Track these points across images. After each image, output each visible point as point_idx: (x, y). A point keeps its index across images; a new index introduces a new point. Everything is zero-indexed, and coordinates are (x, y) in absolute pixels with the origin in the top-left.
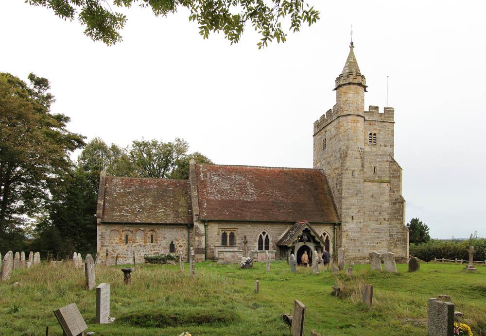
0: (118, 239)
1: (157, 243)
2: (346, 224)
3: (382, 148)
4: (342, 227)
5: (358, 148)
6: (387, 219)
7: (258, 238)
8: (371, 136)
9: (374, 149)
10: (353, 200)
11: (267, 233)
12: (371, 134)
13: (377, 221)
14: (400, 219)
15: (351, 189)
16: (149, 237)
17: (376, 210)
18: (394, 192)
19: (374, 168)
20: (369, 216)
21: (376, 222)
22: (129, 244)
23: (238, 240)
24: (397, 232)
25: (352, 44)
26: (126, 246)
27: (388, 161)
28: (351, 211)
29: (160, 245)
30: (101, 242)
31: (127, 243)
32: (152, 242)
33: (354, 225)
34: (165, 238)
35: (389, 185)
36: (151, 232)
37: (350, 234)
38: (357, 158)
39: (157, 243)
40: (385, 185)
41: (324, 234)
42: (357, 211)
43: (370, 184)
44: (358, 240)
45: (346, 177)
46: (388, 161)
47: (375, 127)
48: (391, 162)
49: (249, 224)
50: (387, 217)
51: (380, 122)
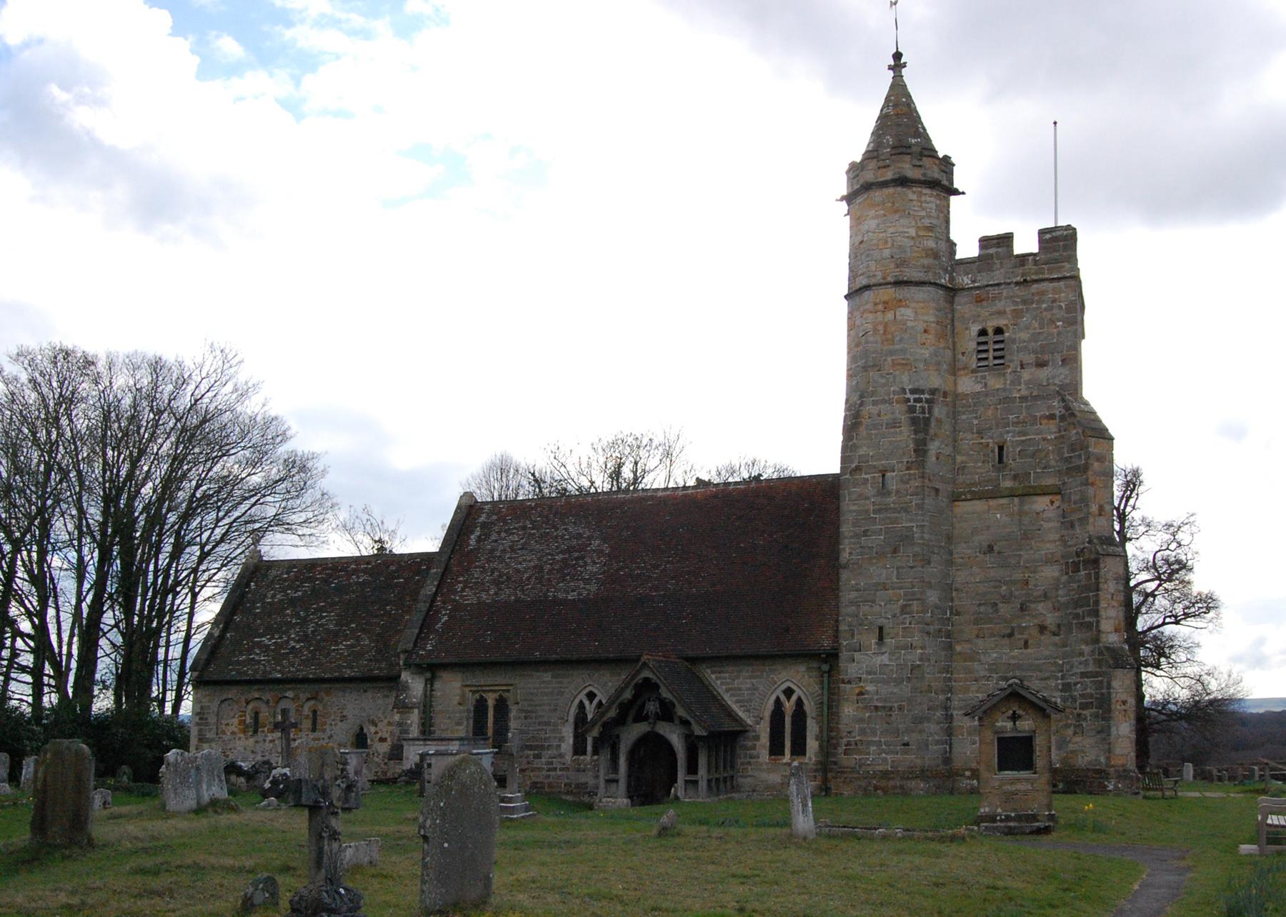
0: (236, 721)
1: (324, 731)
2: (856, 655)
3: (1026, 375)
4: (842, 665)
5: (904, 391)
6: (1053, 628)
7: (573, 710)
8: (983, 339)
9: (995, 383)
10: (881, 572)
11: (798, 692)
12: (983, 333)
13: (1010, 635)
14: (1089, 626)
15: (874, 533)
16: (307, 717)
17: (1006, 599)
18: (1072, 526)
19: (1001, 448)
20: (976, 622)
21: (1006, 641)
22: (260, 736)
23: (516, 718)
24: (1083, 675)
25: (897, 56)
26: (252, 740)
27: (1052, 417)
28: (876, 608)
29: (331, 737)
30: (200, 731)
31: (256, 732)
32: (314, 730)
33: (885, 659)
34: (343, 718)
35: (1057, 504)
36: (312, 702)
37: (870, 688)
38: (894, 424)
39: (324, 731)
40: (1041, 503)
41: (788, 693)
42: (896, 608)
43: (979, 505)
44: (900, 708)
45: (854, 496)
46: (1052, 417)
47: (1000, 305)
48: (1062, 418)
49: (546, 671)
50: (1051, 619)
51: (1017, 283)
